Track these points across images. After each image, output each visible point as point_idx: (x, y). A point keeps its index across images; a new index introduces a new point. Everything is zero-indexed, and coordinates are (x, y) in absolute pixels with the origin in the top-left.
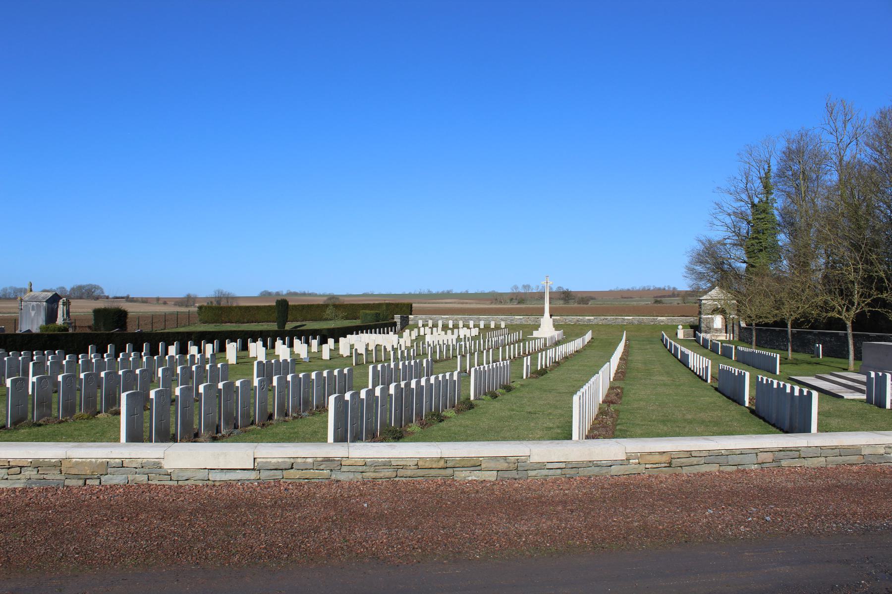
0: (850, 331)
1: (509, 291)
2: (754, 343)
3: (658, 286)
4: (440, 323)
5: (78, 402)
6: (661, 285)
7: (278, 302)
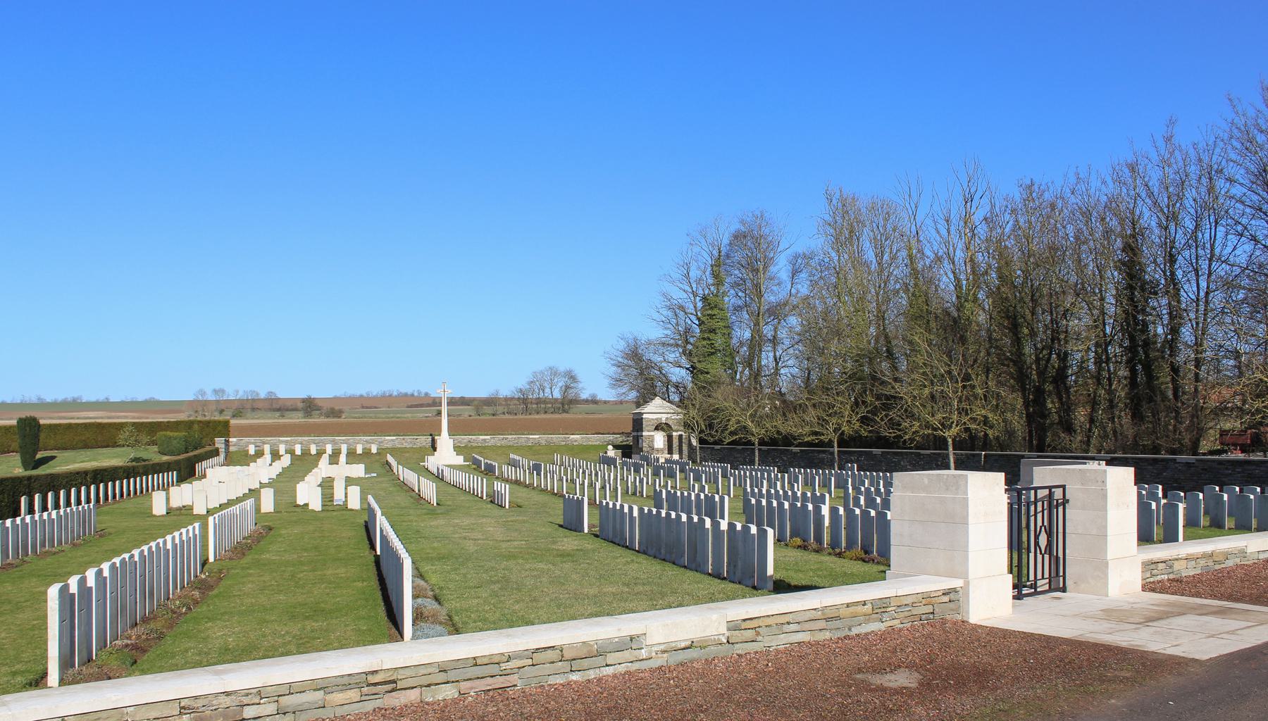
0: (951, 449)
1: (191, 398)
2: (952, 465)
3: (404, 390)
4: (267, 448)
5: (1025, 545)
7: (21, 421)
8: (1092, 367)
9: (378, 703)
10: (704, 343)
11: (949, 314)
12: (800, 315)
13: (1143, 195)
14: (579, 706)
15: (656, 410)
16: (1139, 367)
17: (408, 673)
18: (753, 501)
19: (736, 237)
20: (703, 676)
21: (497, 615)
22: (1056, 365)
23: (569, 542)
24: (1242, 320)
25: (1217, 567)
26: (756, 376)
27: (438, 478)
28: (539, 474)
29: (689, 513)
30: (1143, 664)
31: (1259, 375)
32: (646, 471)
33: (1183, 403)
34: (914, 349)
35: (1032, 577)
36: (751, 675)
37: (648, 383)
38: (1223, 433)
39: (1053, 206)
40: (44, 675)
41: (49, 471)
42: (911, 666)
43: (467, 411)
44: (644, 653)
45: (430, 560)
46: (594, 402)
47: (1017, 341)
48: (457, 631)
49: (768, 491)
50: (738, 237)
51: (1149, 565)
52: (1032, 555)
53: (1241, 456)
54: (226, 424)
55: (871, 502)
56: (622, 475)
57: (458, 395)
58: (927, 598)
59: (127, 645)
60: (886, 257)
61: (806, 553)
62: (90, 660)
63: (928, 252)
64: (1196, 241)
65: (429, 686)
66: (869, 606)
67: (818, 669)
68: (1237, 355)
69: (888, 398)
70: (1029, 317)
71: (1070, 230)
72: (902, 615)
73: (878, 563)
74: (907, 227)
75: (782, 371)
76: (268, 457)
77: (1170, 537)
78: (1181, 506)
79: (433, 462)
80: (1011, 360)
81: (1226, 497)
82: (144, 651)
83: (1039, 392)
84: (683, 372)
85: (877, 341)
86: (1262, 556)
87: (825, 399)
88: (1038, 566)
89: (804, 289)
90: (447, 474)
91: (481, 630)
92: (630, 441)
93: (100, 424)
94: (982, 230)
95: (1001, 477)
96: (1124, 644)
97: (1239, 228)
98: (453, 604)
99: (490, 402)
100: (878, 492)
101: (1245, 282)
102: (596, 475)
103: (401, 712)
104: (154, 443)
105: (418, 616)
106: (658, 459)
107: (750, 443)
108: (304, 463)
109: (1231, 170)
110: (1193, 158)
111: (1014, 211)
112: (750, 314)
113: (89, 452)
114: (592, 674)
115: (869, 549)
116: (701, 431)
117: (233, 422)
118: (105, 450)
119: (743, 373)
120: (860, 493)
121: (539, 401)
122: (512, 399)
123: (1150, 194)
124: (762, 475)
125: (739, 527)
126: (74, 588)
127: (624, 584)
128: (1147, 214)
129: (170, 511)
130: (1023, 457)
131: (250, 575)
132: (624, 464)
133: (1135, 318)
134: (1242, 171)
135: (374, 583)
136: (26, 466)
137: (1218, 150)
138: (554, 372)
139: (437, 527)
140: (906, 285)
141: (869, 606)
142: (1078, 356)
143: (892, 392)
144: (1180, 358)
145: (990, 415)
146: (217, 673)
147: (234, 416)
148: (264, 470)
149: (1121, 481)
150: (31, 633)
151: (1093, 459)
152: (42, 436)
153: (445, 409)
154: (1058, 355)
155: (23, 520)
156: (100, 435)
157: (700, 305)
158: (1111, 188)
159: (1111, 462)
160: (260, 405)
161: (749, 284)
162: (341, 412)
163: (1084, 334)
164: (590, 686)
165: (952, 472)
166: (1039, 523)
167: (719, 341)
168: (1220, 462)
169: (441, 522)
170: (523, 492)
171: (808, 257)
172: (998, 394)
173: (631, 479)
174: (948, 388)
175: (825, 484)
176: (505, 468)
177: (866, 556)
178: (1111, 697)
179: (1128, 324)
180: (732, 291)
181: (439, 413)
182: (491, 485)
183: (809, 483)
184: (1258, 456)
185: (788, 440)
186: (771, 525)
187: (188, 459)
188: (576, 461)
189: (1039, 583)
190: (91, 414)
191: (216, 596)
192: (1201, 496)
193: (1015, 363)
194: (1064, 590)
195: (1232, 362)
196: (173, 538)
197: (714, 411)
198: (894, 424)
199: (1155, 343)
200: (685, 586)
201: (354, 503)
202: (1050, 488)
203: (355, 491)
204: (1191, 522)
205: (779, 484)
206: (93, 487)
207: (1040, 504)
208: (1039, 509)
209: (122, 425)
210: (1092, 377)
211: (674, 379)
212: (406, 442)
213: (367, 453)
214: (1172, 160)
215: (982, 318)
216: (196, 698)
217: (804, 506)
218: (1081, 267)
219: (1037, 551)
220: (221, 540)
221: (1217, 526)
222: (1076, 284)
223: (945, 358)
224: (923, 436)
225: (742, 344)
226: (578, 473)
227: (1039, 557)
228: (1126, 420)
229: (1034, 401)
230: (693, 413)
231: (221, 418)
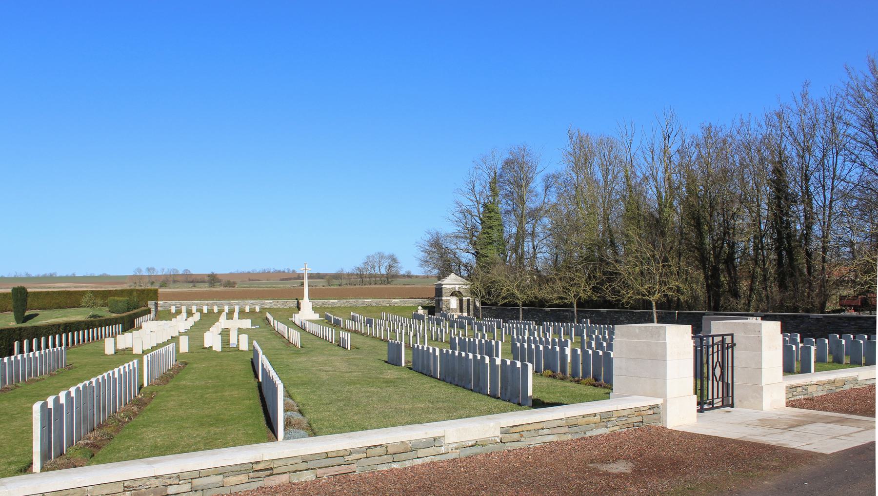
0: (654, 309)
1: (132, 274)
2: (655, 320)
3: (278, 268)
4: (184, 308)
5: (705, 375)
7: (14, 289)
8: (751, 252)
9: (260, 484)
11: (653, 216)
13: (787, 134)
14: (398, 486)
15: (452, 282)
16: (784, 253)
17: (281, 463)
18: (518, 345)
20: (483, 465)
23: (392, 373)
24: (854, 220)
25: (838, 390)
26: (520, 258)
27: (302, 328)
28: (371, 326)
29: (474, 353)
30: (787, 457)
31: (866, 258)
32: (445, 324)
33: (814, 278)
35: (710, 397)
36: (517, 465)
38: (842, 298)
39: (725, 142)
40: (30, 464)
41: (33, 324)
42: (627, 458)
43: (321, 283)
45: (296, 385)
46: (409, 276)
47: (700, 235)
48: (314, 434)
49: (529, 338)
50: (508, 163)
51: (791, 389)
52: (710, 382)
53: (854, 314)
54: (156, 292)
55: (599, 346)
58: (638, 411)
59: (87, 444)
60: (610, 177)
61: (555, 381)
62: (62, 454)
63: (639, 174)
65: (295, 472)
66: (598, 417)
68: (851, 244)
69: (611, 274)
70: (708, 218)
71: (737, 158)
72: (621, 423)
73: (605, 387)
74: (625, 157)
75: (539, 255)
76: (184, 314)
77: (805, 369)
79: (298, 318)
80: (696, 248)
81: (843, 342)
82: (99, 448)
83: (715, 270)
84: (470, 256)
85: (603, 235)
87: (568, 275)
88: (714, 389)
89: (553, 199)
91: (331, 433)
92: (434, 303)
94: (676, 158)
95: (689, 328)
96: (774, 443)
97: (853, 157)
98: (311, 415)
99: (337, 276)
100: (604, 338)
101: (857, 194)
102: (410, 327)
103: (276, 490)
104: (106, 305)
105: (288, 424)
107: (516, 305)
108: (209, 319)
109: (847, 117)
110: (821, 108)
113: (61, 311)
114: (407, 464)
115: (598, 378)
116: (483, 297)
117: (160, 290)
118: (72, 310)
119: (511, 257)
120: (591, 339)
121: (371, 276)
122: (352, 274)
124: (525, 327)
125: (509, 362)
126: (51, 405)
127: (430, 402)
128: (789, 147)
130: (704, 314)
131: (172, 395)
132: (429, 319)
133: (781, 219)
134: (855, 118)
135: (258, 401)
136: (18, 320)
137: (838, 103)
138: (381, 256)
140: (624, 196)
142: (742, 245)
143: (614, 270)
144: (812, 247)
145: (681, 286)
146: (149, 463)
148: (182, 324)
151: (752, 315)
152: (29, 300)
153: (306, 281)
154: (728, 244)
155: (16, 357)
157: (482, 210)
158: (765, 130)
159: (764, 318)
160: (179, 279)
161: (515, 195)
162: (234, 283)
163: (746, 230)
164: (406, 471)
165: (655, 325)
166: (715, 360)
167: (495, 234)
168: (840, 318)
169: (303, 359)
170: (360, 339)
171: (556, 177)
173: (434, 329)
174: (653, 267)
175: (568, 333)
176: (347, 322)
177: (596, 382)
178: (765, 479)
179: (777, 223)
180: (504, 200)
181: (302, 284)
183: (557, 332)
185: (542, 303)
186: (531, 361)
187: (130, 316)
189: (715, 401)
190: (63, 285)
191: (149, 410)
192: (827, 341)
193: (698, 249)
194: (732, 406)
195: (848, 249)
196: (119, 370)
197: (492, 283)
198: (615, 292)
199: (795, 236)
200: (472, 403)
201: (244, 346)
202: (723, 336)
203: (244, 338)
204: (820, 359)
207: (716, 347)
208: (715, 350)
210: (752, 259)
211: (464, 261)
212: (279, 304)
213: (252, 311)
215: (676, 218)
216: (135, 480)
217: (553, 348)
219: (714, 379)
221: (837, 362)
222: (741, 196)
224: (635, 300)
225: (510, 237)
228: (775, 289)
229: (711, 276)
230: (477, 284)
231: (153, 288)
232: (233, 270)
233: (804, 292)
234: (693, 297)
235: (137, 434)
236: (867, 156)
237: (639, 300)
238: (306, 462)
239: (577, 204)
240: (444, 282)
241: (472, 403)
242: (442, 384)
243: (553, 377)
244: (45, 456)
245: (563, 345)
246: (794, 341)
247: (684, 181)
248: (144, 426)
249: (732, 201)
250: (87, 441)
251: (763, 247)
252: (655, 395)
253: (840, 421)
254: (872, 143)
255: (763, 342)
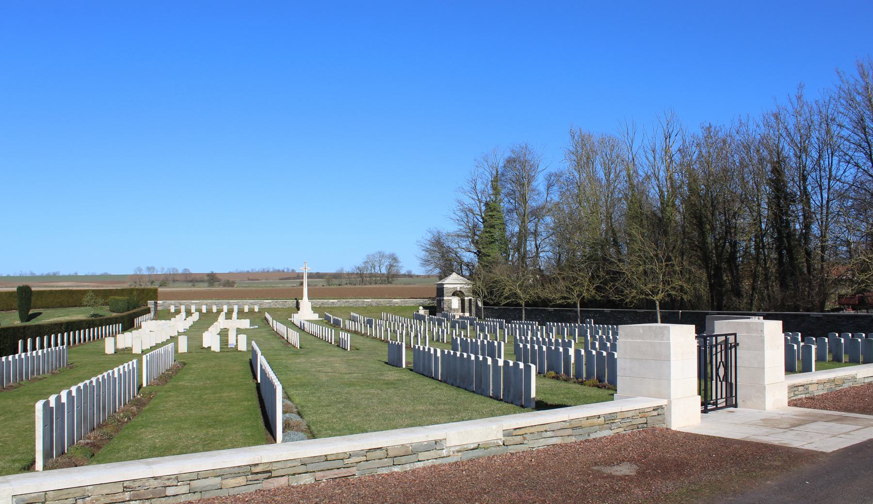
0: (658, 308)
1: (132, 273)
2: (659, 320)
4: (183, 308)
5: (709, 375)
6: (280, 267)
7: (19, 288)
8: (753, 252)
9: (258, 487)
10: (487, 235)
11: (655, 215)
12: (553, 215)
13: (784, 135)
14: (399, 489)
15: (453, 282)
16: (784, 252)
17: (279, 465)
18: (521, 346)
19: (508, 161)
20: (486, 468)
21: (342, 425)
22: (723, 250)
23: (392, 374)
24: (851, 220)
25: (838, 389)
26: (523, 257)
27: (301, 329)
28: (371, 327)
29: (476, 354)
30: (789, 456)
31: (863, 257)
32: (446, 324)
33: (814, 277)
34: (632, 239)
35: (714, 398)
36: (520, 468)
37: (447, 262)
38: (840, 297)
39: (724, 142)
40: (33, 462)
41: (37, 323)
42: (631, 460)
43: (321, 282)
44: (444, 453)
45: (295, 386)
46: (410, 276)
47: (702, 234)
48: (313, 436)
49: (532, 339)
50: (510, 161)
51: (793, 388)
52: (714, 382)
53: (852, 312)
54: (155, 291)
55: (603, 346)
56: (429, 327)
57: (314, 271)
58: (642, 412)
59: (88, 444)
60: (612, 176)
61: (558, 382)
62: (63, 453)
63: (641, 173)
64: (819, 166)
65: (294, 474)
66: (602, 419)
67: (567, 463)
68: (848, 243)
69: (615, 273)
70: (710, 217)
71: (737, 158)
72: (625, 425)
73: (608, 389)
74: (627, 156)
75: (541, 254)
76: (183, 314)
77: (807, 368)
78: (814, 347)
79: (297, 318)
80: (698, 247)
81: (842, 340)
82: (99, 448)
83: (718, 269)
84: (472, 255)
85: (606, 234)
86: (867, 381)
87: (571, 274)
88: (718, 389)
89: (556, 198)
90: (307, 326)
91: (330, 436)
92: (435, 303)
93: (71, 291)
94: (677, 158)
95: (692, 328)
96: (776, 443)
97: (847, 158)
98: (310, 417)
99: (337, 276)
100: (608, 339)
101: (852, 194)
102: (411, 327)
103: (275, 492)
104: (107, 304)
105: (287, 426)
106: (454, 316)
107: (519, 305)
108: (208, 319)
109: (840, 119)
110: (816, 111)
111: (698, 145)
112: (519, 215)
113: (64, 310)
114: (408, 467)
115: (602, 379)
116: (485, 297)
117: (160, 290)
118: (74, 309)
119: (513, 256)
120: (595, 339)
121: (371, 275)
122: (352, 274)
123: (789, 134)
124: (528, 327)
125: (511, 364)
126: (53, 404)
127: (431, 404)
128: (787, 148)
129: (117, 351)
130: (707, 314)
131: (171, 396)
132: (431, 319)
133: (781, 218)
134: (848, 120)
135: (256, 402)
136: (23, 319)
137: (831, 106)
138: (382, 255)
139: (300, 364)
140: (626, 195)
141: (602, 419)
142: (744, 244)
143: (617, 269)
144: (812, 246)
145: (685, 285)
146: (148, 464)
147: (161, 286)
148: (181, 323)
149: (773, 329)
150: (25, 434)
151: (755, 315)
152: (33, 298)
153: (305, 281)
154: (730, 243)
155: (20, 356)
156: (70, 298)
157: (483, 208)
158: (763, 130)
159: (767, 317)
160: (178, 278)
161: (517, 194)
162: (234, 283)
163: (747, 229)
164: (407, 475)
165: (659, 325)
166: (719, 360)
167: (497, 234)
168: (839, 317)
169: (302, 360)
170: (359, 340)
171: (558, 176)
172: (690, 270)
173: (436, 330)
174: (656, 266)
175: (572, 334)
176: (347, 322)
177: (600, 384)
178: (767, 479)
179: (776, 222)
180: (506, 199)
181: (302, 284)
182: (337, 334)
183: (560, 333)
184: (863, 313)
185: (545, 302)
186: (534, 362)
187: (130, 315)
188: (397, 317)
189: (719, 401)
190: (66, 284)
191: (148, 410)
192: (826, 340)
193: (701, 249)
194: (736, 406)
195: (845, 248)
196: (119, 370)
197: (494, 282)
198: (619, 291)
199: (795, 235)
200: (474, 405)
201: (243, 346)
202: (726, 335)
203: (243, 338)
204: (820, 358)
205: (539, 333)
206: (66, 334)
207: (719, 347)
208: (719, 350)
209: (85, 292)
210: (753, 259)
211: (465, 260)
212: (279, 303)
213: (251, 311)
214: (802, 112)
215: (678, 218)
216: (134, 480)
217: (557, 349)
218: (744, 183)
219: (717, 380)
220: (151, 372)
221: (837, 361)
222: (741, 195)
223: (653, 245)
224: (639, 300)
225: (513, 236)
226: (398, 326)
227: (719, 383)
228: (776, 288)
229: (715, 275)
230: (479, 283)
231: (152, 287)
232: (233, 269)
233: (804, 291)
234: (696, 296)
235: (136, 435)
236: (861, 157)
237: (643, 299)
238: (305, 464)
239: (580, 203)
240: (446, 282)
241: (474, 405)
242: (443, 385)
243: (557, 378)
244: (47, 455)
245: (567, 345)
246: (795, 340)
247: (686, 181)
248: (143, 427)
249: (733, 200)
250: (87, 441)
251: (764, 246)
252: (661, 397)
253: (840, 420)
254: (864, 144)
255: (765, 341)
